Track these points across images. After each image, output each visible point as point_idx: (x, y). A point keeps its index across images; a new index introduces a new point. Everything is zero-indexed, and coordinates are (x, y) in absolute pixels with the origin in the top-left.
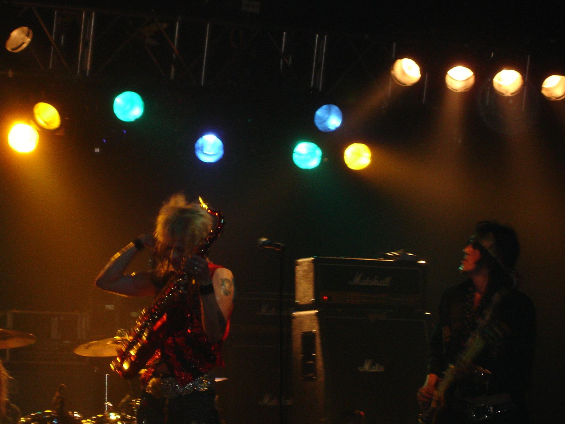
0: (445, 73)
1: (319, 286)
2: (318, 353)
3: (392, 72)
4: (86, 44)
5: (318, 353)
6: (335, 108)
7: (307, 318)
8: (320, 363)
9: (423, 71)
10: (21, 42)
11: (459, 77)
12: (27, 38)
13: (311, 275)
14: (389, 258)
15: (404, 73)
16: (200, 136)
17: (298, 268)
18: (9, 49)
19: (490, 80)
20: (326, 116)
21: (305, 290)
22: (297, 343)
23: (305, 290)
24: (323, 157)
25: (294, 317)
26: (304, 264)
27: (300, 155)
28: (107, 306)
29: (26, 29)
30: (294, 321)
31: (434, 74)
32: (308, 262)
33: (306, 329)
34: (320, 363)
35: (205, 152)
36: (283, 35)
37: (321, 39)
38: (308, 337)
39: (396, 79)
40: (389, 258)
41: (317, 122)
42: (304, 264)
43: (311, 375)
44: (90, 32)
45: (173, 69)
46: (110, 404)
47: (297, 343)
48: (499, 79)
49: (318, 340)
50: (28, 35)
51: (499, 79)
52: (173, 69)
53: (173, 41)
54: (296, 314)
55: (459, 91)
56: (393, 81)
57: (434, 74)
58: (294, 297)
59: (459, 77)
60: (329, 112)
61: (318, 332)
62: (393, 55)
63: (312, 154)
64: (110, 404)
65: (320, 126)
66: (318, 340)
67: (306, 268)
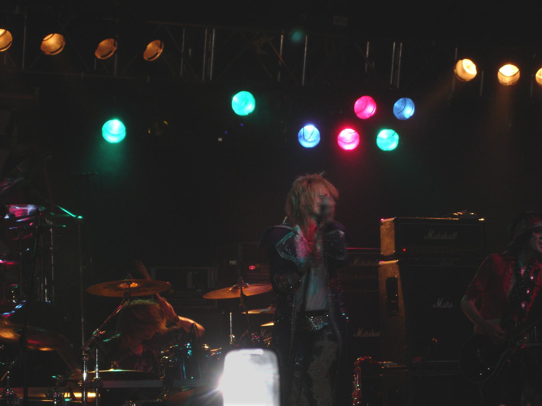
0: (497, 71)
1: (399, 242)
2: (400, 294)
3: (455, 71)
4: (209, 55)
5: (400, 294)
6: (409, 101)
8: (401, 302)
9: (478, 69)
10: (155, 52)
11: (508, 73)
12: (159, 49)
13: (393, 232)
14: (456, 217)
15: (464, 71)
16: (302, 126)
17: (382, 227)
18: (146, 58)
19: (533, 75)
20: (403, 107)
21: (388, 244)
23: (388, 244)
24: (400, 141)
25: (380, 266)
27: (382, 139)
28: (231, 262)
29: (159, 42)
31: (489, 70)
32: (390, 222)
33: (389, 275)
34: (401, 302)
35: (112, 132)
36: (266, 307)
37: (397, 46)
38: (391, 282)
39: (458, 76)
40: (456, 217)
41: (395, 112)
44: (211, 44)
45: (279, 74)
46: (233, 337)
48: (540, 75)
49: (399, 283)
50: (161, 48)
51: (540, 75)
52: (279, 74)
53: (279, 51)
54: (382, 263)
55: (508, 84)
56: (456, 78)
57: (489, 70)
58: (379, 251)
59: (508, 73)
60: (405, 104)
61: (399, 278)
62: (456, 57)
63: (391, 137)
64: (233, 337)
65: (397, 116)
66: (399, 283)
67: (389, 227)
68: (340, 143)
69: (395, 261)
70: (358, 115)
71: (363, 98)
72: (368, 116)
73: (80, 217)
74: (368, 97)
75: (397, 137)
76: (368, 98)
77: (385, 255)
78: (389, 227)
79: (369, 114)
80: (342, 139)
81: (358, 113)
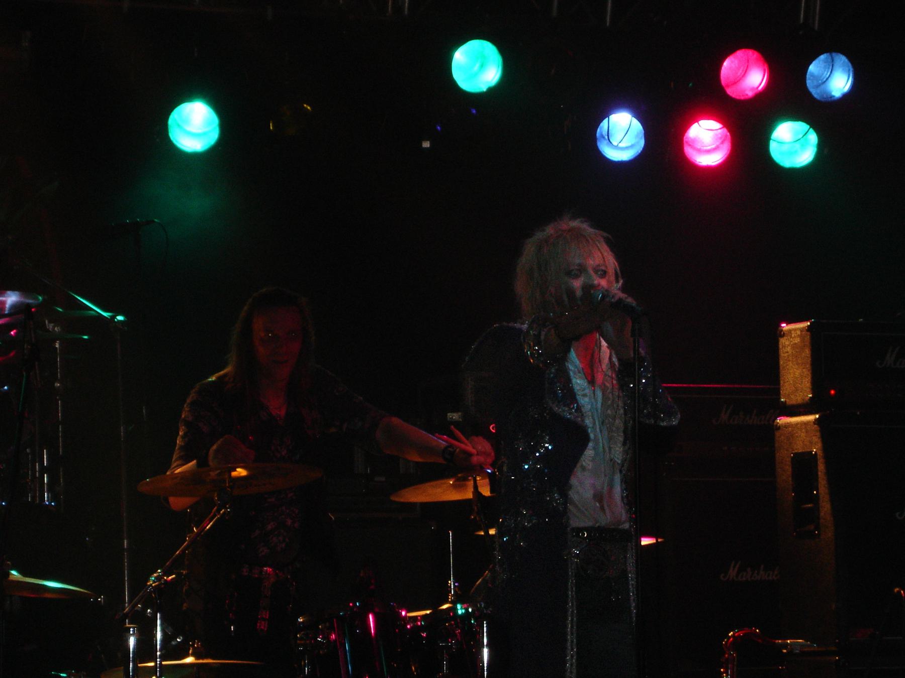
2: (822, 489)
5: (822, 489)
7: (800, 427)
21: (796, 378)
22: (785, 473)
23: (796, 378)
25: (778, 428)
26: (794, 331)
30: (777, 434)
33: (799, 448)
34: (826, 507)
35: (189, 129)
38: (804, 462)
42: (794, 331)
43: (812, 527)
47: (785, 473)
49: (821, 467)
54: (782, 421)
61: (820, 453)
66: (821, 467)
67: (797, 340)
68: (689, 151)
69: (811, 418)
70: (730, 91)
71: (740, 53)
72: (750, 94)
73: (120, 318)
74: (750, 52)
75: (813, 138)
76: (752, 54)
77: (789, 402)
78: (797, 340)
79: (752, 89)
80: (692, 143)
81: (728, 86)
